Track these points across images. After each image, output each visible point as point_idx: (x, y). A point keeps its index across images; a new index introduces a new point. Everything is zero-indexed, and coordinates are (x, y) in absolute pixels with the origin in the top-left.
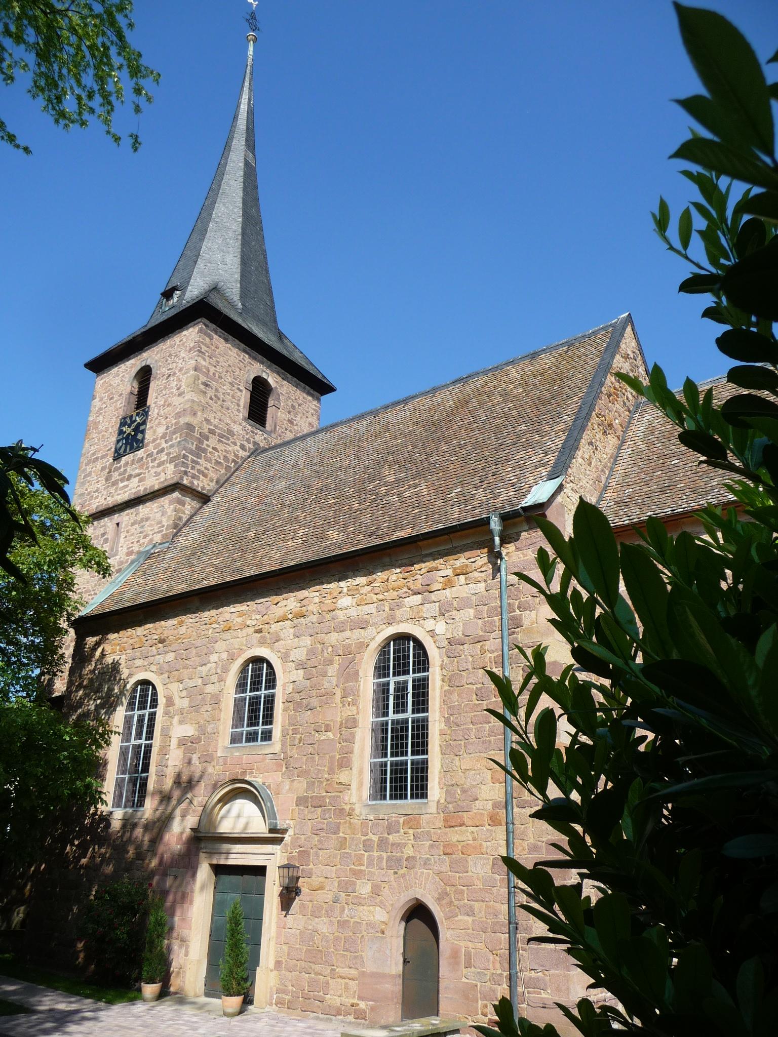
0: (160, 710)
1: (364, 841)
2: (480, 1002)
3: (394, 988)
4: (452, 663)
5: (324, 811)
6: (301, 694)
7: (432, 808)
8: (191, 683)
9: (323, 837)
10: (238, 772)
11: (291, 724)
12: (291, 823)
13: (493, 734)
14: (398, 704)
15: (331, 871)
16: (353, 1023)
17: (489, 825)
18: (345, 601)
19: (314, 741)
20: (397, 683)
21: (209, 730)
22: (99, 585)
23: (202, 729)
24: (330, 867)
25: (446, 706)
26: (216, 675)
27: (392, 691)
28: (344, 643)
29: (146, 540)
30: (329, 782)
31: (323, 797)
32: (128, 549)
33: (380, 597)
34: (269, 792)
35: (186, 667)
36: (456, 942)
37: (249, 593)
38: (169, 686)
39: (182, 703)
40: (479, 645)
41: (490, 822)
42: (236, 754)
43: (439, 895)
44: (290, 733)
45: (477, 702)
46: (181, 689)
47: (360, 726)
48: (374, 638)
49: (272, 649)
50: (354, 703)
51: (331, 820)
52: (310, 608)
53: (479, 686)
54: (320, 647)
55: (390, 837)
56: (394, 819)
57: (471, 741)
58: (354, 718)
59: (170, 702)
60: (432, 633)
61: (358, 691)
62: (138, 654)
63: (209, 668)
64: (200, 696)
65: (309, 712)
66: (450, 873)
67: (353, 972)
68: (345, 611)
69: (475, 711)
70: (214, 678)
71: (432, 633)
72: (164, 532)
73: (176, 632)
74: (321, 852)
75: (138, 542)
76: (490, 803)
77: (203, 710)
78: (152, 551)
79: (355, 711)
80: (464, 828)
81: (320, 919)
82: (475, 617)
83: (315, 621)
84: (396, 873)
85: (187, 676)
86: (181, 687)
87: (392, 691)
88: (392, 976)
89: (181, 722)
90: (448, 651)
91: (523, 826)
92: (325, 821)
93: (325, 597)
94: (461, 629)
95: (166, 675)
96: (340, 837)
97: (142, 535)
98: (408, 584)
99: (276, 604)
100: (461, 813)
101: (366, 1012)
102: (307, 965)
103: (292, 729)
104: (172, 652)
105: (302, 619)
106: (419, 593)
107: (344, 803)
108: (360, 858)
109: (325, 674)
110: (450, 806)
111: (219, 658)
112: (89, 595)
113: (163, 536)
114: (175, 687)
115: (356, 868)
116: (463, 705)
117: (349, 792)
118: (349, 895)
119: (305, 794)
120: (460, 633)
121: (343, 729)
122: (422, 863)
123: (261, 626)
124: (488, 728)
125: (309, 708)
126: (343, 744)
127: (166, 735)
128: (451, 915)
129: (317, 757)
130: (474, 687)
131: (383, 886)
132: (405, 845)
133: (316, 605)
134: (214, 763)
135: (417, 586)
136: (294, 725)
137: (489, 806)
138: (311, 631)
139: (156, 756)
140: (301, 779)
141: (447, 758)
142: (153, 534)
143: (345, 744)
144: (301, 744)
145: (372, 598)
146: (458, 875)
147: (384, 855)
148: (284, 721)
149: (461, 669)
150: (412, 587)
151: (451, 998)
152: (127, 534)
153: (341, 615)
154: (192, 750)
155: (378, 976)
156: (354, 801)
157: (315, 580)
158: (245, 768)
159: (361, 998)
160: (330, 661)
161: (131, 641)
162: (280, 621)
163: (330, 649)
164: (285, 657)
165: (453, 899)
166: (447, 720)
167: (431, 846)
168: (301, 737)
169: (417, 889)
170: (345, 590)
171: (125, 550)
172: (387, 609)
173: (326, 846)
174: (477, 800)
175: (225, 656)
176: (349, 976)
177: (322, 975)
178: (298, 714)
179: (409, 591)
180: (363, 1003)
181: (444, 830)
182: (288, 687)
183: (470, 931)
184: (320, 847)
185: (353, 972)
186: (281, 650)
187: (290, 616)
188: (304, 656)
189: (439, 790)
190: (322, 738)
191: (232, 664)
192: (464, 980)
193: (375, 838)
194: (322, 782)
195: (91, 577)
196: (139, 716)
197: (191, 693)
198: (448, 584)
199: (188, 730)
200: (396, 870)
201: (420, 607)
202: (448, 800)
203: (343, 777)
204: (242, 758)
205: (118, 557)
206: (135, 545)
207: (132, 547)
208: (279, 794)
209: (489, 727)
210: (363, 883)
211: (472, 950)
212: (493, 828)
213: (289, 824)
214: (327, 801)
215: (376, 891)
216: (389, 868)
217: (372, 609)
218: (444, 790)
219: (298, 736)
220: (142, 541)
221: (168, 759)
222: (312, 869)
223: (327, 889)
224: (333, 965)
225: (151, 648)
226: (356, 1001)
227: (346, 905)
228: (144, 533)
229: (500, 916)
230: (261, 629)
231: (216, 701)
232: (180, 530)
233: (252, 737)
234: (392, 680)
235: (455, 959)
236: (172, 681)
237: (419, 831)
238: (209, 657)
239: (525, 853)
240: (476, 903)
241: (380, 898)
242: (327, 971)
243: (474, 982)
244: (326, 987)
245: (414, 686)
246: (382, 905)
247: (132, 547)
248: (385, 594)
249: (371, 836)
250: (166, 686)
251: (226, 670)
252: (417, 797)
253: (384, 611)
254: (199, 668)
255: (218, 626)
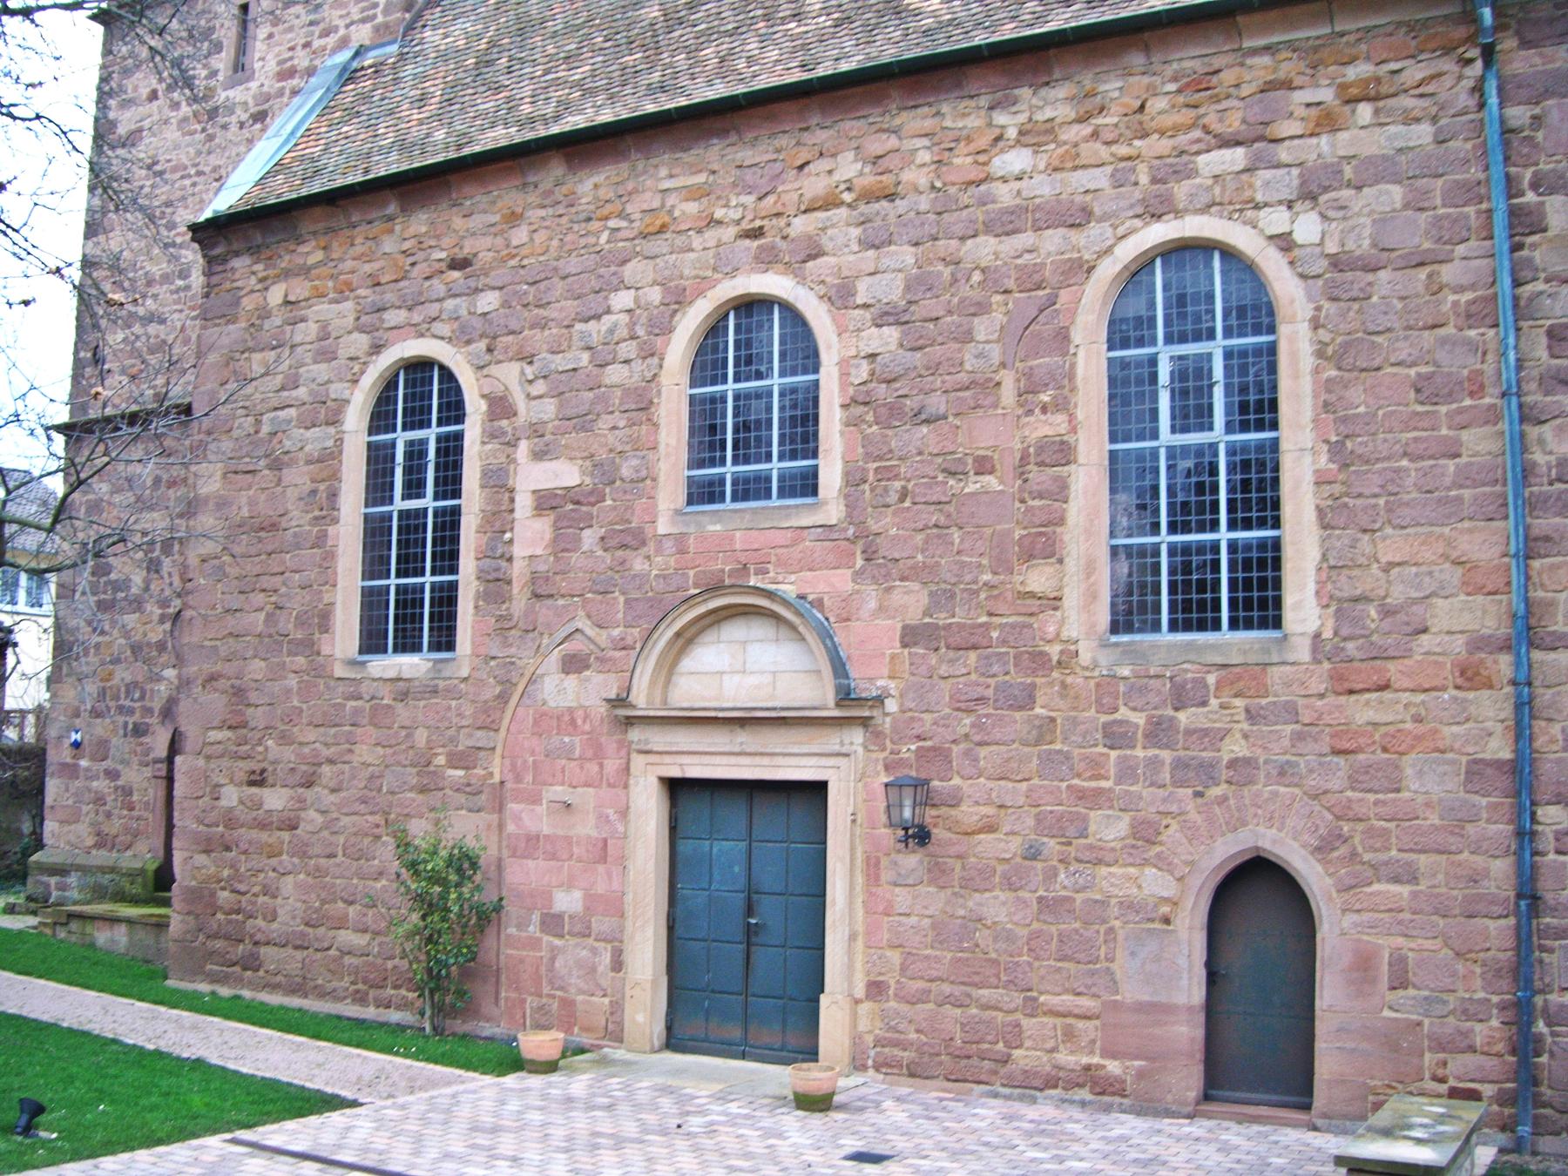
0: (472, 430)
1: (1106, 726)
2: (1427, 1056)
3: (1188, 1032)
4: (1343, 315)
5: (987, 657)
6: (897, 385)
7: (1303, 653)
8: (560, 362)
9: (986, 716)
10: (723, 571)
11: (868, 456)
12: (892, 685)
13: (1468, 482)
14: (419, 472)
15: (1012, 792)
16: (1090, 1102)
17: (1457, 687)
18: (1015, 160)
19: (944, 493)
20: (410, 444)
21: (626, 471)
22: (209, 153)
23: (605, 473)
24: (1010, 785)
25: (1332, 416)
26: (634, 343)
27: (400, 458)
28: (1019, 261)
29: (331, 41)
30: (996, 592)
31: (981, 625)
32: (280, 63)
33: (1123, 150)
34: (819, 616)
35: (542, 325)
36: (1365, 938)
37: (715, 141)
38: (494, 370)
39: (539, 409)
40: (1422, 274)
41: (1459, 681)
42: (711, 528)
43: (1322, 838)
44: (871, 477)
45: (1420, 408)
46: (530, 377)
47: (1081, 460)
48: (1108, 251)
49: (801, 279)
50: (1062, 405)
51: (1007, 678)
52: (908, 176)
53: (1424, 369)
54: (947, 272)
55: (1182, 717)
56: (1189, 675)
57: (1406, 497)
58: (1063, 443)
59: (500, 407)
60: (1284, 242)
61: (1071, 376)
62: (390, 297)
63: (608, 325)
64: (591, 394)
65: (924, 429)
66: (1349, 793)
67: (1086, 1003)
68: (1016, 185)
69: (1415, 429)
70: (628, 349)
71: (1284, 242)
72: (380, 19)
73: (499, 241)
74: (983, 752)
75: (307, 45)
76: (1460, 641)
77: (604, 423)
78: (355, 65)
79: (1066, 425)
80: (1387, 695)
81: (987, 895)
82: (1406, 206)
83: (924, 207)
84: (1199, 794)
85: (545, 347)
86: (530, 372)
87: (400, 458)
88: (1190, 1009)
89: (538, 455)
90: (1331, 285)
91: (1550, 691)
92: (991, 681)
93: (951, 149)
94: (1367, 232)
95: (482, 345)
96: (1037, 716)
97: (317, 30)
98: (1205, 120)
99: (801, 167)
100: (1378, 662)
101: (1124, 1081)
102: (958, 990)
103: (876, 469)
104: (494, 288)
105: (884, 203)
106: (1238, 143)
107: (1042, 639)
108: (1096, 768)
109: (967, 337)
110: (1350, 645)
111: (637, 300)
112: (182, 177)
113: (377, 29)
114: (509, 374)
115: (1085, 784)
116: (1380, 413)
117: (1058, 613)
118: (1070, 844)
119: (927, 620)
120: (1366, 243)
121: (1029, 467)
122: (1275, 772)
123: (758, 223)
124: (1452, 469)
125: (923, 417)
126: (1031, 503)
127: (498, 482)
128: (1353, 881)
129: (956, 536)
130: (1412, 372)
131: (1164, 822)
132: (1225, 733)
133: (926, 170)
134: (651, 548)
135: (1233, 124)
136: (880, 458)
137: (1458, 644)
138: (915, 234)
139: (473, 535)
140: (915, 586)
141: (1339, 537)
142: (347, 26)
143: (1037, 503)
144: (907, 504)
145: (1096, 152)
146: (1371, 797)
147: (1166, 755)
148: (849, 448)
149: (1372, 328)
150: (1217, 127)
151: (1353, 1050)
152: (275, 30)
153: (1005, 195)
154: (580, 520)
155: (1158, 1010)
156: (1074, 635)
157: (915, 107)
158: (742, 559)
159: (1109, 1053)
160: (979, 304)
161: (368, 268)
162: (815, 209)
163: (977, 277)
164: (840, 296)
165: (1360, 849)
166: (1336, 450)
167: (1298, 737)
168: (904, 488)
169: (1261, 829)
170: (1012, 133)
171: (272, 66)
172: (1144, 179)
173: (997, 734)
174: (1425, 631)
175: (655, 295)
176: (1076, 1011)
177: (1001, 1010)
178: (890, 432)
179: (1209, 137)
180: (1116, 1063)
181: (1331, 699)
182: (857, 366)
183: (1407, 916)
184: (977, 738)
185: (1086, 1003)
186: (828, 279)
187: (847, 197)
188: (899, 292)
189: (1317, 611)
190: (967, 490)
191: (679, 315)
192: (1387, 1013)
193: (1139, 719)
194: (977, 592)
195: (184, 135)
196: (410, 444)
197: (561, 385)
198: (1326, 122)
199: (565, 474)
200: (1199, 788)
201: (1244, 177)
202: (1345, 632)
203: (1038, 579)
204: (732, 539)
205: (254, 85)
206: (300, 52)
207: (291, 58)
208: (848, 620)
209: (1457, 466)
210: (1109, 817)
211: (1410, 954)
212: (1471, 695)
213: (885, 689)
214: (995, 634)
215: (1145, 834)
216: (1179, 783)
217: (1098, 179)
218: (1332, 609)
219: (898, 485)
220: (317, 44)
221: (511, 541)
222: (959, 788)
223: (1006, 828)
224: (1030, 990)
225: (427, 284)
226: (1096, 1060)
227: (1061, 867)
228: (322, 26)
229: (1485, 883)
230: (761, 228)
231: (642, 404)
232: (419, 16)
233: (751, 489)
234: (401, 439)
235: (1366, 970)
236: (501, 357)
237: (1264, 702)
238: (606, 298)
239: (1555, 748)
240: (1423, 857)
241: (1158, 849)
242: (1018, 999)
243: (1414, 1017)
244: (1014, 1037)
245: (438, 451)
246: (1162, 863)
247: (291, 58)
248: (1137, 143)
249: (1123, 713)
250: (485, 371)
251: (665, 329)
252: (1249, 625)
253: (1136, 184)
254: (579, 326)
255: (624, 224)
